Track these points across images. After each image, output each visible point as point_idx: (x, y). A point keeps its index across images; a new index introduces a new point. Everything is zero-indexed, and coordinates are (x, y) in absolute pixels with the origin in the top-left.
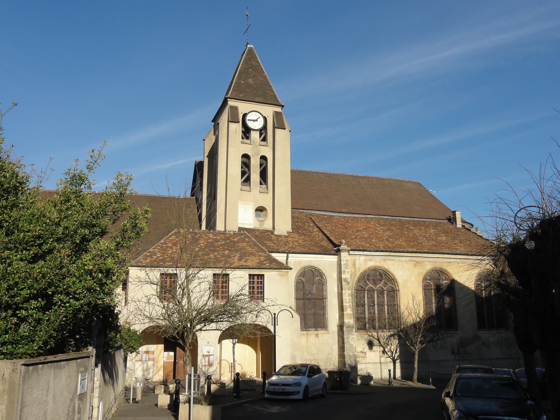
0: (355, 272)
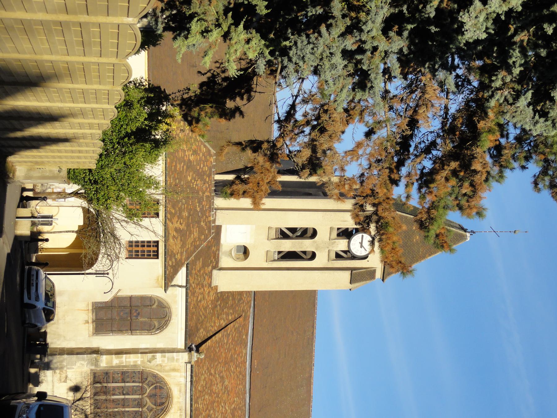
0: (165, 371)
